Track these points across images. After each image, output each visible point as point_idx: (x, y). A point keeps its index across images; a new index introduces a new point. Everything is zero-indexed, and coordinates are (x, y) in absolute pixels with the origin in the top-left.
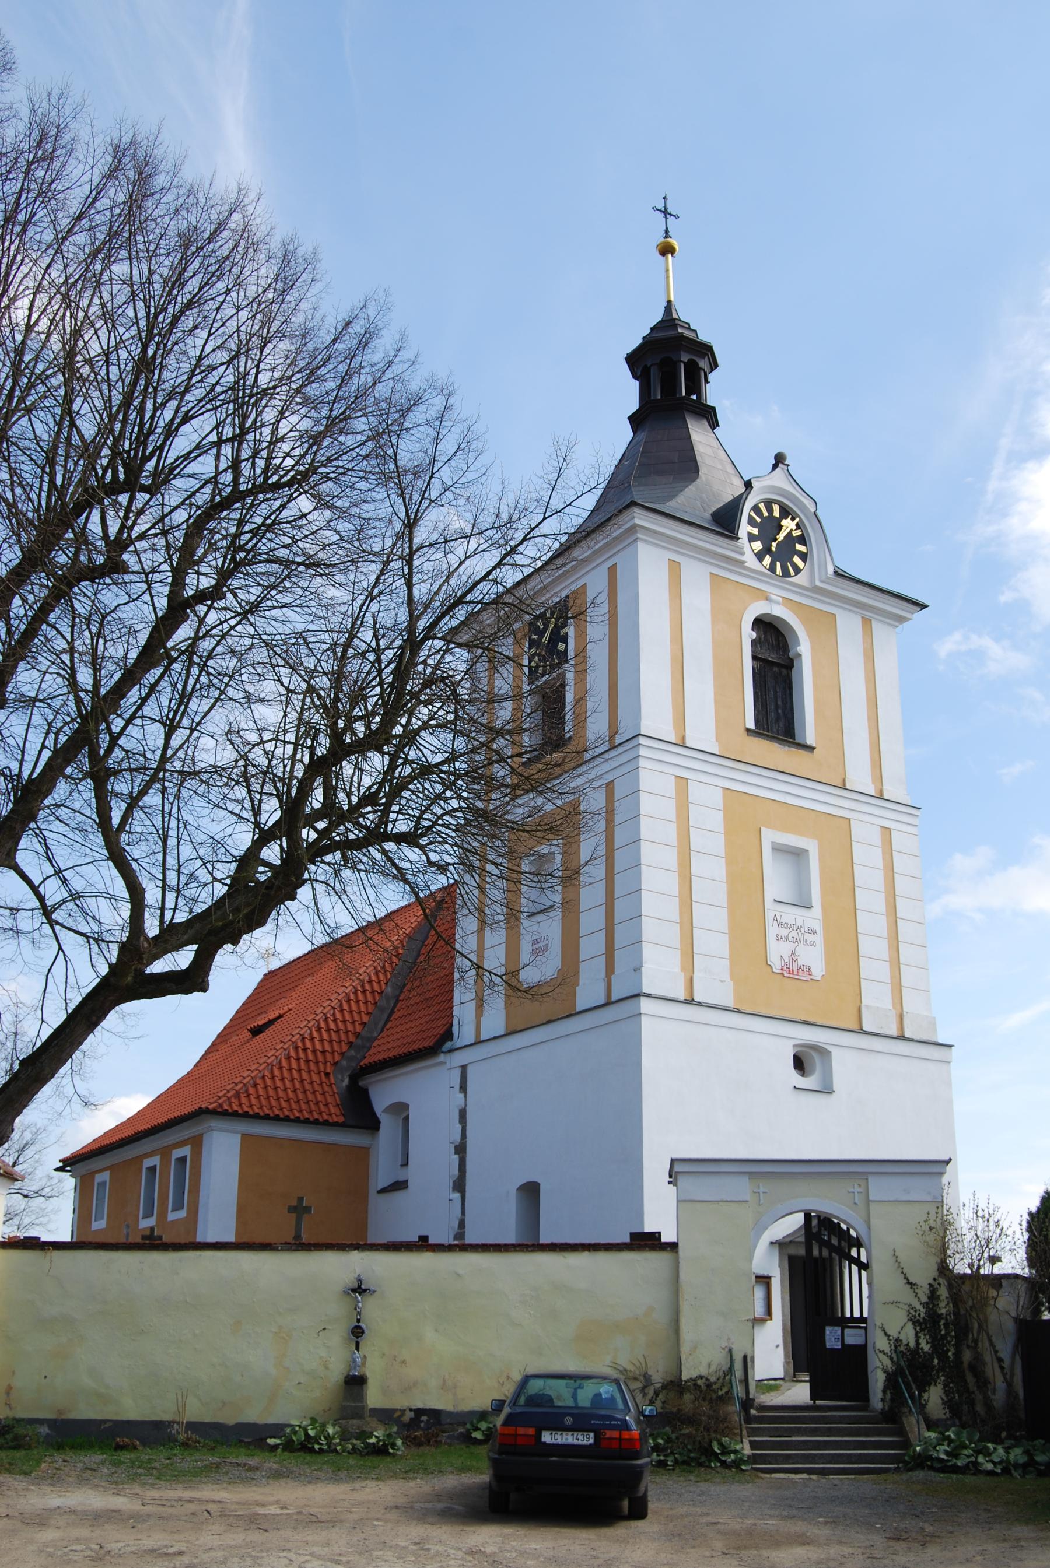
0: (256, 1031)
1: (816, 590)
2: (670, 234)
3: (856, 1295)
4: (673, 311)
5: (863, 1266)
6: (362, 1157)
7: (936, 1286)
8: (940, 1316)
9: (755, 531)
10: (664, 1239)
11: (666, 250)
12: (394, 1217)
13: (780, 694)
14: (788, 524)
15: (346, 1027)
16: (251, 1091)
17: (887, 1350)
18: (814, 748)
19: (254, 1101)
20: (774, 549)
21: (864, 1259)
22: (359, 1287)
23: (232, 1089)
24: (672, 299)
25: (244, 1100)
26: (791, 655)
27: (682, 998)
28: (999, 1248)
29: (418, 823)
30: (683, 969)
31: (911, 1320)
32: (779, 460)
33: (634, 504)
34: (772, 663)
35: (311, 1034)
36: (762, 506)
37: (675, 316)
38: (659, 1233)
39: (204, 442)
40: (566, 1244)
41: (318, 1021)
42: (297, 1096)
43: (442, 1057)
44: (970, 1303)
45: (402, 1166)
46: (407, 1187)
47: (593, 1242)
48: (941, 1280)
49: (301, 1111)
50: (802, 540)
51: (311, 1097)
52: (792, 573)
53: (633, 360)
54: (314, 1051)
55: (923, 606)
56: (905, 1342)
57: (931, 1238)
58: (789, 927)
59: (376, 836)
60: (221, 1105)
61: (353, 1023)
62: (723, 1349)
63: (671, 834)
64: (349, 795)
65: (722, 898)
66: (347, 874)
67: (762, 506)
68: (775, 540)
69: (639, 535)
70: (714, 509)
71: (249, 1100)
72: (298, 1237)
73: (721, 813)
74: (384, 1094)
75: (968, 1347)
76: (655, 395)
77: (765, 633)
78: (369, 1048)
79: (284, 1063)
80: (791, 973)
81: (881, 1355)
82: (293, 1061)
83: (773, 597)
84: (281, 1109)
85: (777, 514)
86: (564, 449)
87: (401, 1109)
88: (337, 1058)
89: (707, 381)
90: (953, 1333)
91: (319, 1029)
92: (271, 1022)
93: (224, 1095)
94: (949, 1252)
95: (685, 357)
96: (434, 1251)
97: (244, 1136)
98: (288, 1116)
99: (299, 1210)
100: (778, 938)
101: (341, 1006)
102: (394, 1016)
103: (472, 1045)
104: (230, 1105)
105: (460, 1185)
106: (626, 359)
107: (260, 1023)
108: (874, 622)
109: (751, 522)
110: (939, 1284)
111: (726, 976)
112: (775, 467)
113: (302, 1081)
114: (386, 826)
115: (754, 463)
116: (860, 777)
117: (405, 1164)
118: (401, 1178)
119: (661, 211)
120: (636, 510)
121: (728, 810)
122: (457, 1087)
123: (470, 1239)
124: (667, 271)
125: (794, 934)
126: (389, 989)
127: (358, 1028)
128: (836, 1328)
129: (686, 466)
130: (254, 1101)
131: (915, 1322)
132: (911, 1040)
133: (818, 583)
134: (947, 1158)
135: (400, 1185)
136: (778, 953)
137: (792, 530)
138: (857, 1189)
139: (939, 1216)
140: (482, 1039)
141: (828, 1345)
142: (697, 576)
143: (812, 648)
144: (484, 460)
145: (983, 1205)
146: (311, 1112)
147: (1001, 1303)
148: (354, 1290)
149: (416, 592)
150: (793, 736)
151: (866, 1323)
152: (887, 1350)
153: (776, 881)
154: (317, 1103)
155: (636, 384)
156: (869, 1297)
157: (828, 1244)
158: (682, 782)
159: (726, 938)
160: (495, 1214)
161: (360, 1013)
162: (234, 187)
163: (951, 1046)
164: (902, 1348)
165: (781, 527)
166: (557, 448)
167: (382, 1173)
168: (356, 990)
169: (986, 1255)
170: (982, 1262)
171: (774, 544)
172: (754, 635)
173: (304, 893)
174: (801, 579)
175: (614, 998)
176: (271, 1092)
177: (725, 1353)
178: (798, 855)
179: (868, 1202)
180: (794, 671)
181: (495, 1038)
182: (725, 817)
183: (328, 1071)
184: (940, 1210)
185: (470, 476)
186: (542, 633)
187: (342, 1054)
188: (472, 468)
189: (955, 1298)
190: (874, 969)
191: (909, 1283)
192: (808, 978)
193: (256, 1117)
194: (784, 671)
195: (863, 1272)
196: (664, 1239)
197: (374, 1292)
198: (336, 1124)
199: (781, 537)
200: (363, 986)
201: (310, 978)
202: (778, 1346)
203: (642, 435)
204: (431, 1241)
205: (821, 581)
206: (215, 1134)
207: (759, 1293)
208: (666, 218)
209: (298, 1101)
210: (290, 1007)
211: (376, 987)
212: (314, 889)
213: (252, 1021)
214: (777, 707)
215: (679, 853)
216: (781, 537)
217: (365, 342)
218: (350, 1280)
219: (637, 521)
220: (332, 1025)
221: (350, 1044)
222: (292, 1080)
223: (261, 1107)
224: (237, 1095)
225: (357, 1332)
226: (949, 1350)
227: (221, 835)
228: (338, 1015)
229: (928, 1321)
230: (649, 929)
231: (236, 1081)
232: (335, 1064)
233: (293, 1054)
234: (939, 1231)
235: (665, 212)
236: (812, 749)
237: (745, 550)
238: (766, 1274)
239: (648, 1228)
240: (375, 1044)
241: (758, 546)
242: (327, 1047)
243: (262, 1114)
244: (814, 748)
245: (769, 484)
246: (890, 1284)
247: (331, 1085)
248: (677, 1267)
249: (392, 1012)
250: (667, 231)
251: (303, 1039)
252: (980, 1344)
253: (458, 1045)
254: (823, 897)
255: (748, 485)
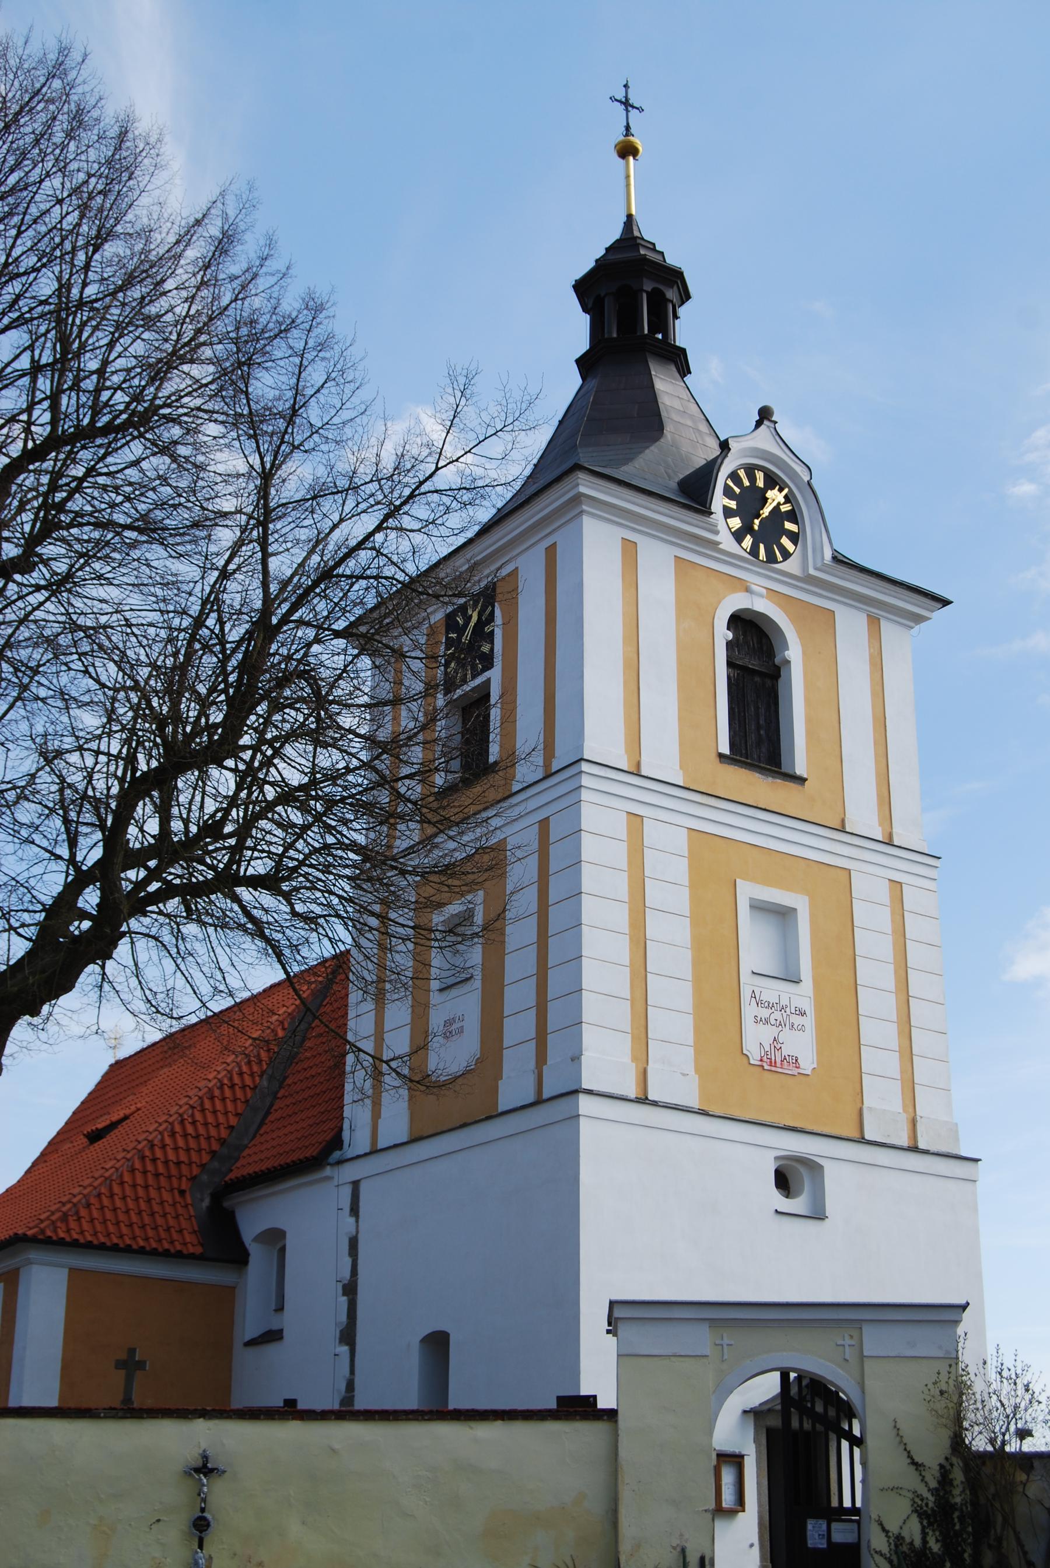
0: (95, 1137)
1: (809, 579)
2: (632, 131)
3: (851, 1479)
4: (635, 228)
5: (856, 1442)
6: (226, 1299)
7: (948, 1467)
8: (953, 1507)
9: (733, 505)
10: (601, 1404)
11: (627, 150)
12: (262, 1376)
13: (762, 711)
14: (775, 496)
15: (208, 1131)
16: (83, 1212)
17: (885, 1550)
18: (805, 780)
19: (86, 1226)
20: (756, 527)
21: (857, 1432)
22: (205, 1466)
23: (58, 1210)
24: (633, 212)
25: (73, 1225)
26: (777, 661)
27: (633, 1096)
28: (1029, 1419)
29: (279, 864)
30: (634, 1059)
31: (916, 1511)
32: (765, 415)
33: (577, 467)
34: (753, 672)
35: (162, 1140)
36: (742, 473)
37: (636, 233)
38: (595, 1397)
39: (9, 370)
40: (473, 1410)
41: (172, 1124)
42: (142, 1219)
43: (328, 1171)
44: (992, 1490)
45: (276, 1310)
46: (281, 1338)
47: (508, 1408)
48: (954, 1460)
49: (147, 1239)
50: (793, 516)
51: (160, 1221)
52: (780, 558)
53: (584, 288)
54: (166, 1162)
55: (945, 603)
56: (908, 1540)
57: (940, 1405)
58: (770, 1006)
59: (227, 881)
60: (43, 1231)
61: (218, 1126)
62: (674, 1548)
63: (620, 885)
64: (186, 822)
65: (686, 970)
66: (191, 929)
67: (742, 473)
68: (758, 516)
69: (584, 507)
70: (681, 477)
71: (80, 1225)
72: (127, 1399)
73: (686, 861)
74: (254, 1219)
75: (990, 1546)
76: (610, 332)
77: (745, 634)
78: (237, 1159)
79: (127, 1178)
80: (773, 1064)
81: (877, 1557)
82: (138, 1174)
83: (754, 588)
84: (121, 1237)
85: (760, 483)
86: (462, 380)
87: (275, 1238)
88: (196, 1171)
89: (676, 317)
90: (970, 1529)
91: (173, 1134)
92: (113, 1126)
93: (48, 1218)
94: (966, 1424)
95: (648, 286)
96: (302, 1419)
97: (73, 1272)
98: (130, 1246)
99: (130, 1365)
100: (757, 1020)
101: (202, 1104)
102: (271, 1118)
103: (366, 1155)
104: (55, 1231)
105: (348, 1336)
106: (574, 287)
107: (100, 1126)
108: (883, 623)
109: (728, 492)
110: (952, 1465)
111: (690, 1069)
112: (759, 424)
113: (149, 1201)
114: (239, 867)
115: (734, 420)
116: (863, 816)
117: (280, 1309)
118: (275, 1327)
119: (620, 101)
120: (581, 475)
121: (694, 858)
122: (347, 1209)
123: (360, 1404)
124: (628, 177)
125: (777, 1015)
126: (265, 1083)
127: (224, 1133)
128: (821, 1521)
129: (648, 422)
130: (86, 1226)
131: (920, 1512)
132: (926, 1152)
133: (812, 571)
134: (963, 1302)
135: (273, 1336)
136: (756, 1039)
137: (779, 504)
138: (848, 1341)
139: (953, 1377)
140: (380, 1146)
141: (810, 1544)
142: (657, 560)
143: (804, 653)
144: (364, 394)
145: (1008, 1363)
146: (109, 1235)
147: (1032, 1490)
148: (197, 1470)
149: (273, 563)
150: (778, 764)
151: (859, 1515)
152: (885, 1550)
153: (756, 947)
154: (168, 1229)
155: (587, 318)
156: (863, 1481)
157: (811, 1414)
158: (635, 820)
159: (689, 1020)
160: (391, 1371)
161: (226, 1113)
162: (53, 46)
163: (977, 1160)
164: (905, 1548)
165: (766, 500)
166: (453, 378)
167: (251, 1320)
168: (222, 1085)
169: (1012, 1428)
170: (1007, 1437)
171: (757, 522)
172: (730, 635)
173: (123, 948)
174: (791, 566)
175: (545, 1096)
176: (109, 1215)
177: (676, 1553)
178: (783, 915)
179: (862, 1357)
180: (781, 682)
181: (396, 1146)
182: (690, 866)
183: (184, 1187)
184: (953, 1370)
185: (345, 415)
186: (461, 630)
187: (203, 1166)
188: (348, 405)
189: (973, 1484)
190: (879, 1061)
191: (914, 1463)
192: (795, 1072)
193: (89, 1246)
194: (769, 682)
195: (857, 1451)
196: (601, 1404)
197: (224, 1472)
198: (192, 1257)
199: (766, 512)
200: (231, 1079)
201: (165, 1070)
202: (752, 1545)
203: (593, 383)
204: (301, 1406)
205: (816, 569)
206: (35, 1268)
207: (728, 1477)
208: (627, 111)
209: (143, 1227)
210: (139, 1105)
211: (248, 1080)
212: (132, 943)
213: (92, 1125)
214: (759, 727)
215: (630, 910)
216: (766, 512)
217: (223, 245)
218: (191, 1456)
219: (582, 489)
220: (190, 1130)
221: (213, 1153)
222: (137, 1199)
223: (95, 1234)
224: (65, 1218)
225: (201, 1525)
226: (965, 1551)
227: (26, 875)
228: (198, 1116)
229: (936, 1514)
230: (591, 1007)
231: (64, 1199)
232: (193, 1179)
233: (138, 1165)
234: (952, 1396)
235: (626, 104)
236: (801, 780)
237: (719, 528)
238: (737, 1451)
239: (584, 1391)
240: (245, 1154)
241: (736, 523)
242: (183, 1157)
243: (96, 1242)
244: (805, 780)
245: (749, 446)
246: (891, 1465)
247: (186, 1206)
248: (617, 1441)
249: (268, 1113)
250: (628, 128)
251: (152, 1147)
252: (1005, 1544)
253: (350, 1154)
254: (815, 967)
255: (725, 446)
